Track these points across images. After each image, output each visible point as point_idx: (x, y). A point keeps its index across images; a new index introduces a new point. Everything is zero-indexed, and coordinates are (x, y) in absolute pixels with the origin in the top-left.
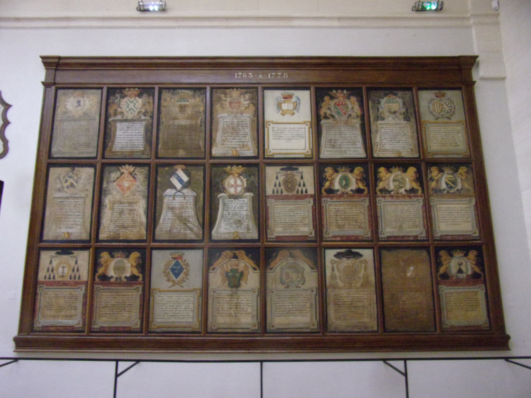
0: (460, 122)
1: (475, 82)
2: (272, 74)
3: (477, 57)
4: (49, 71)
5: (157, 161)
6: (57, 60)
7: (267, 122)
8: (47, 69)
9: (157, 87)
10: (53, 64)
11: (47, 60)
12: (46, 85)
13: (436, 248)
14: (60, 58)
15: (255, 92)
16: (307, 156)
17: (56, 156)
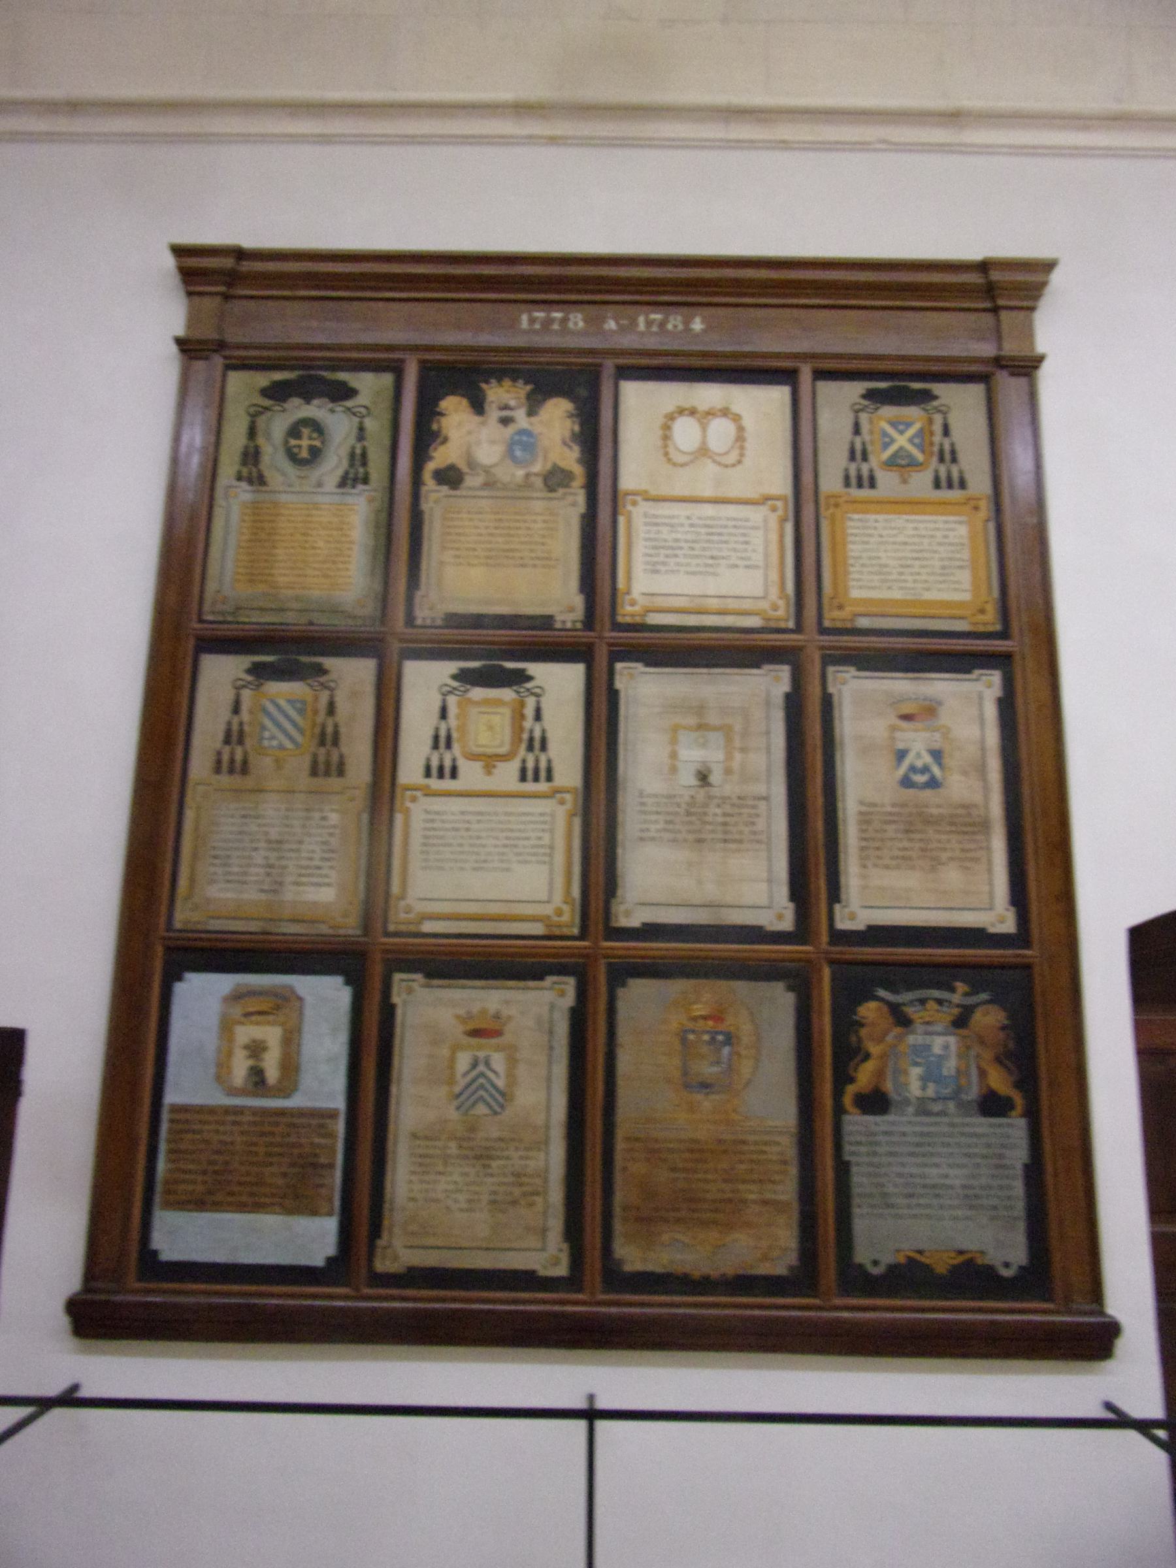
0: (767, 498)
1: (1040, 359)
2: (653, 316)
3: (1048, 266)
4: (196, 299)
5: (826, 640)
6: (228, 263)
7: (627, 494)
8: (190, 294)
9: (609, 365)
10: (208, 273)
11: (193, 262)
12: (188, 348)
13: (842, 981)
14: (240, 254)
15: (583, 386)
16: (773, 624)
17: (210, 618)
